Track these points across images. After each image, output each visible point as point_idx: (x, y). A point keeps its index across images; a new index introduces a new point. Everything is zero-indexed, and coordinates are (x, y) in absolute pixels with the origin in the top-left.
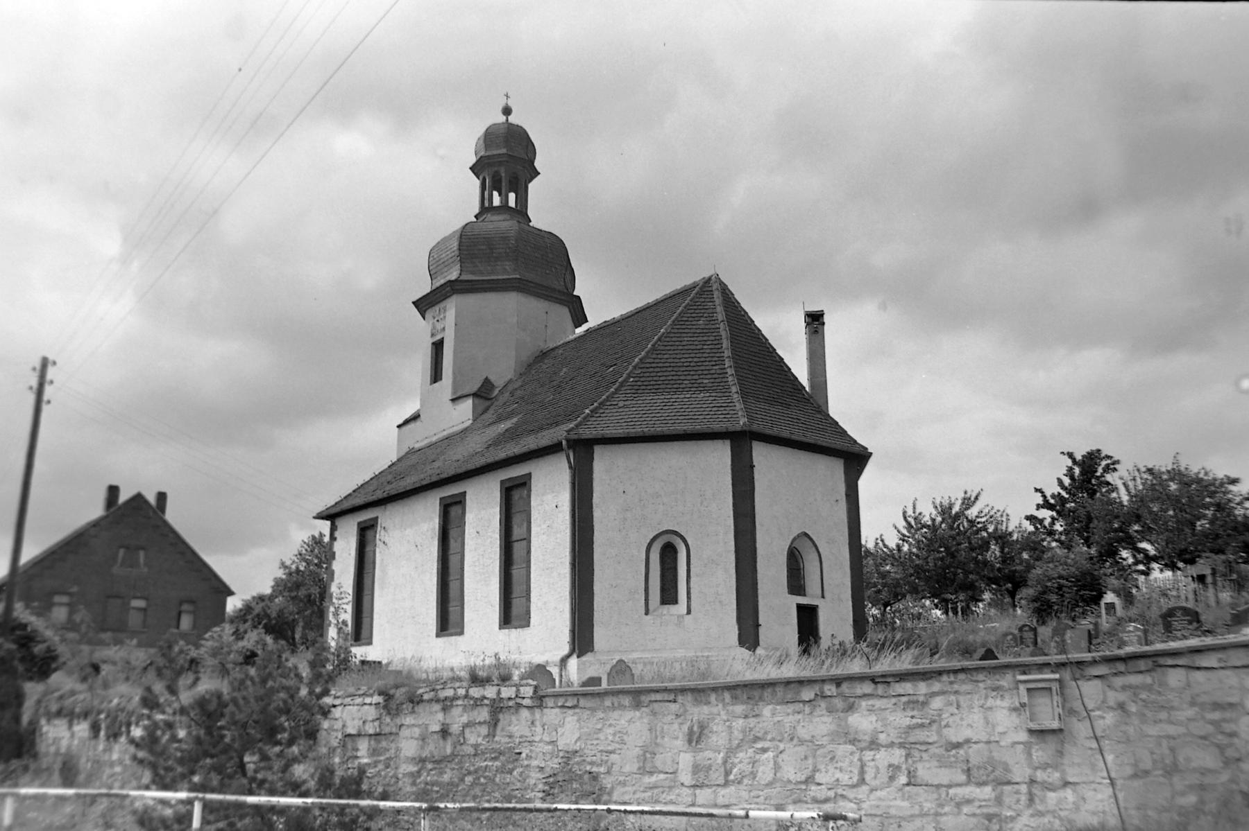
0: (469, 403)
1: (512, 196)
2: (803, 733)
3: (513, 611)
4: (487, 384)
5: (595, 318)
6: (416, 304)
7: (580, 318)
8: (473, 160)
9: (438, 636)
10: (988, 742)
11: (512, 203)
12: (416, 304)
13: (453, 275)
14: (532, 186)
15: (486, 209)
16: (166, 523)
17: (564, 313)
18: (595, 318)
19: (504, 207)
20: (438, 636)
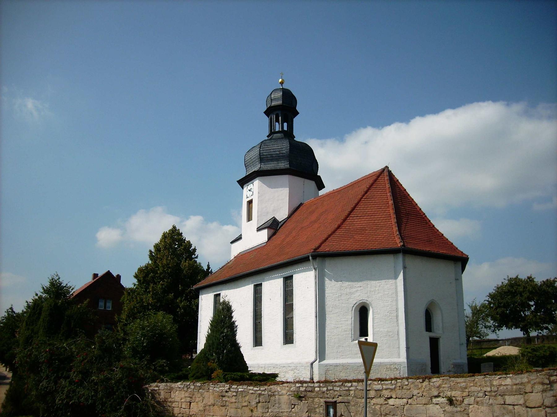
0: (265, 231)
1: (285, 125)
2: (503, 383)
3: (288, 338)
4: (274, 220)
5: (330, 186)
6: (239, 182)
7: (320, 186)
8: (265, 109)
9: (174, 227)
10: (526, 393)
11: (285, 128)
12: (239, 182)
13: (256, 169)
14: (296, 120)
15: (272, 132)
16: (254, 374)
17: (312, 184)
18: (330, 186)
19: (283, 131)
20: (174, 227)
